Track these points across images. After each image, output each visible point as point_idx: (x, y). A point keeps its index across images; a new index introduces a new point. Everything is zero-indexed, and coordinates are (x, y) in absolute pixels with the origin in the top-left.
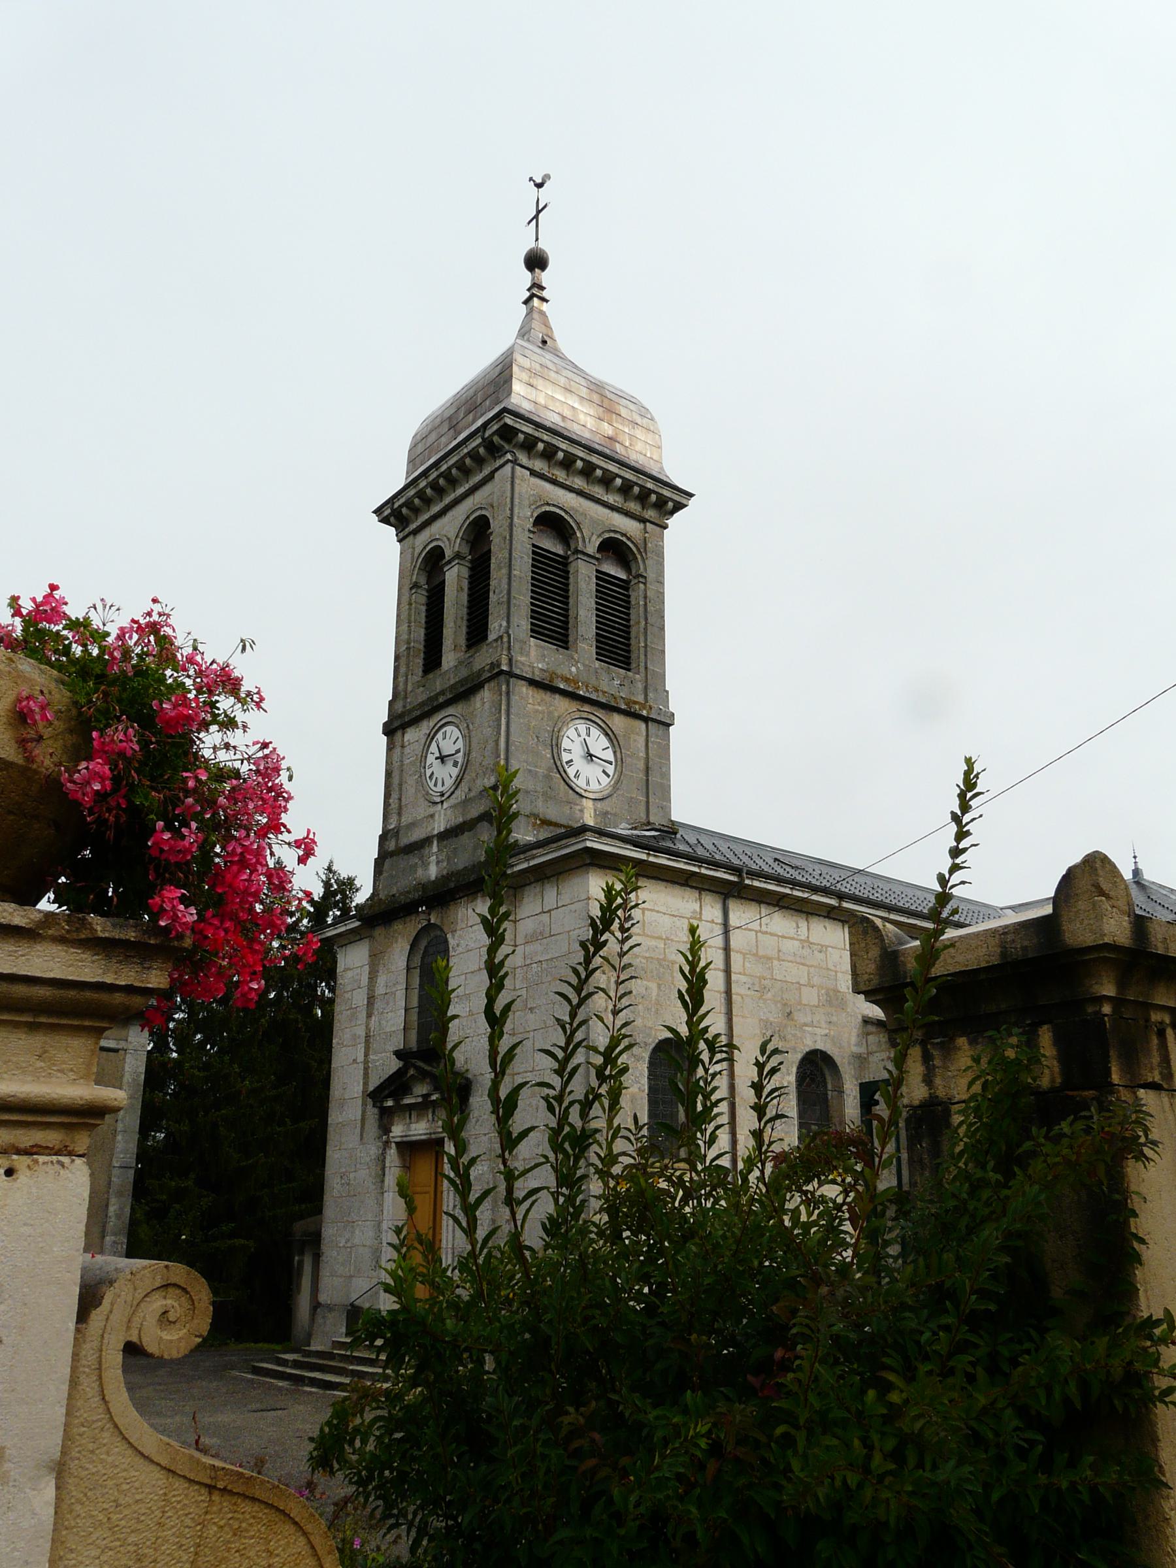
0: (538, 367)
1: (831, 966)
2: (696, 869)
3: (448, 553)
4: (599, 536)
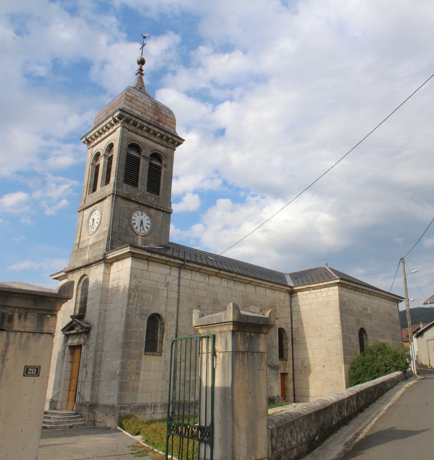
2: (169, 259)
3: (102, 154)
4: (151, 152)
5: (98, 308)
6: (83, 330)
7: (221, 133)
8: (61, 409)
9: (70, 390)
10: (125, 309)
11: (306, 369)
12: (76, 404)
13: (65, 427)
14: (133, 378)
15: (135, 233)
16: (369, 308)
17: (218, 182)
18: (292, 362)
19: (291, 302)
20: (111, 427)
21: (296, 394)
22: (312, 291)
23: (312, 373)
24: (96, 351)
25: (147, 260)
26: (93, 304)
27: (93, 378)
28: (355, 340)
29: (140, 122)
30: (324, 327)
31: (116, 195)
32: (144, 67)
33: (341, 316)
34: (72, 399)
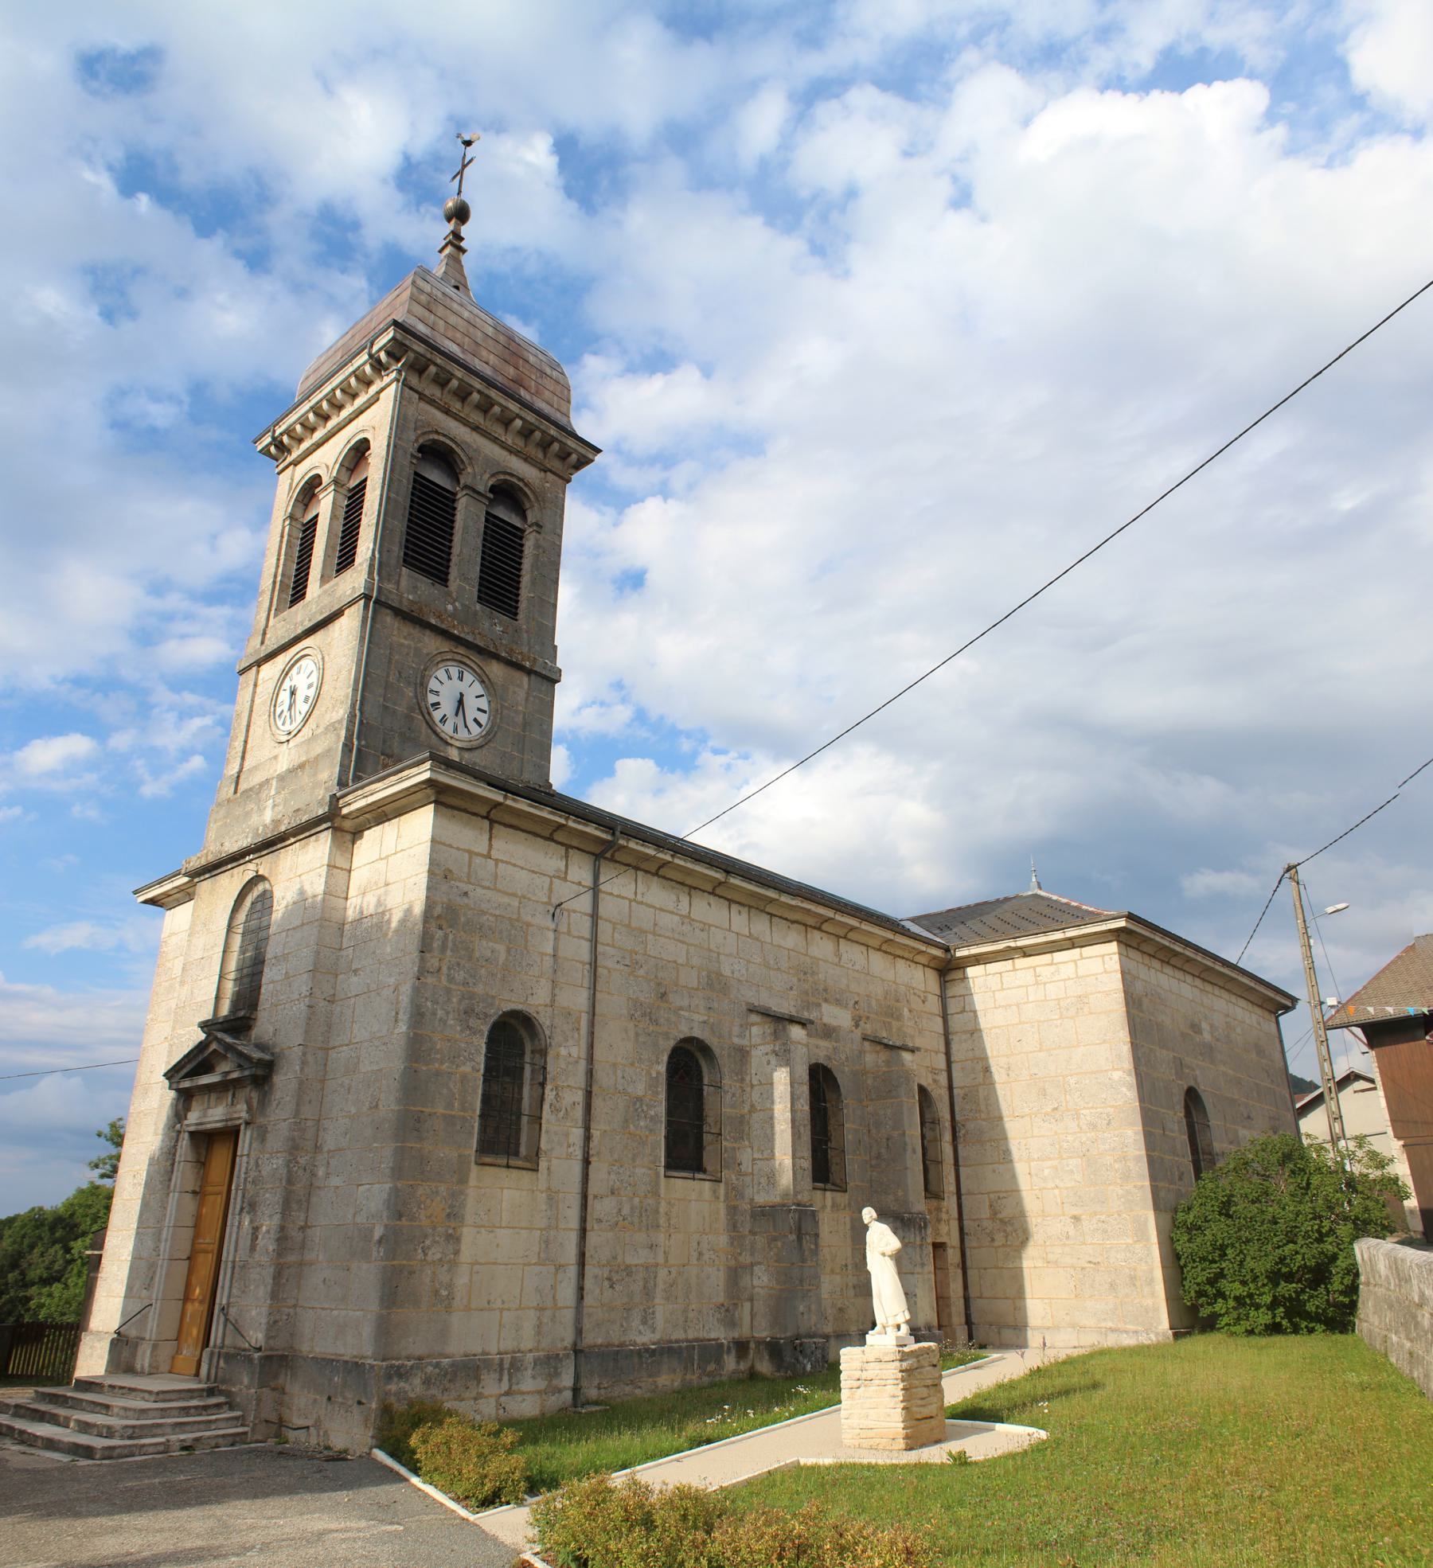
0: (439, 294)
1: (712, 947)
2: (563, 821)
3: (326, 480)
4: (493, 476)
5: (305, 990)
6: (247, 1073)
7: (633, 581)
8: (153, 1371)
9: (186, 1298)
10: (406, 989)
11: (1013, 1231)
12: (212, 1354)
13: (166, 1447)
14: (434, 1254)
15: (437, 735)
16: (1205, 1026)
17: (622, 714)
18: (955, 1206)
19: (943, 998)
20: (346, 1451)
21: (974, 1319)
22: (1021, 962)
23: (1031, 1243)
24: (294, 1148)
25: (487, 818)
26: (287, 976)
27: (280, 1252)
28: (1176, 1128)
29: (459, 373)
30: (1072, 1081)
31: (377, 603)
32: (464, 230)
33: (1134, 1046)
34: (195, 1332)
